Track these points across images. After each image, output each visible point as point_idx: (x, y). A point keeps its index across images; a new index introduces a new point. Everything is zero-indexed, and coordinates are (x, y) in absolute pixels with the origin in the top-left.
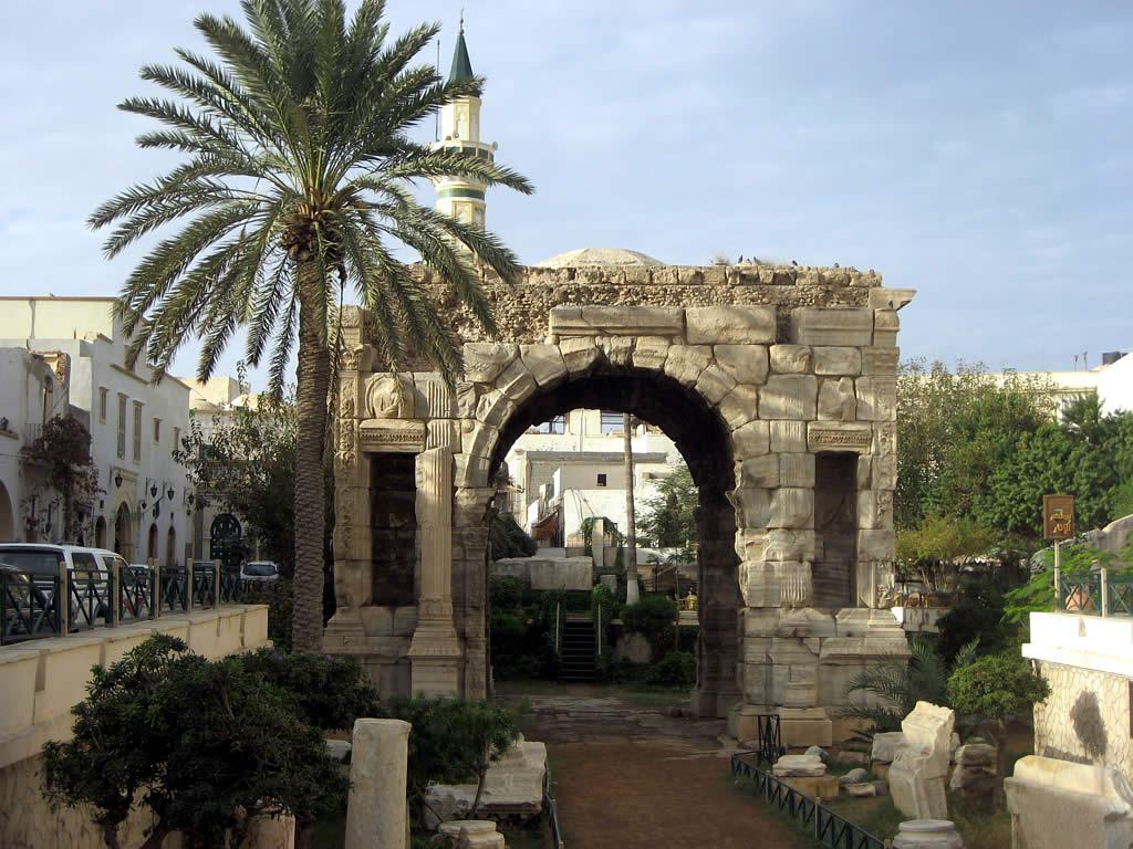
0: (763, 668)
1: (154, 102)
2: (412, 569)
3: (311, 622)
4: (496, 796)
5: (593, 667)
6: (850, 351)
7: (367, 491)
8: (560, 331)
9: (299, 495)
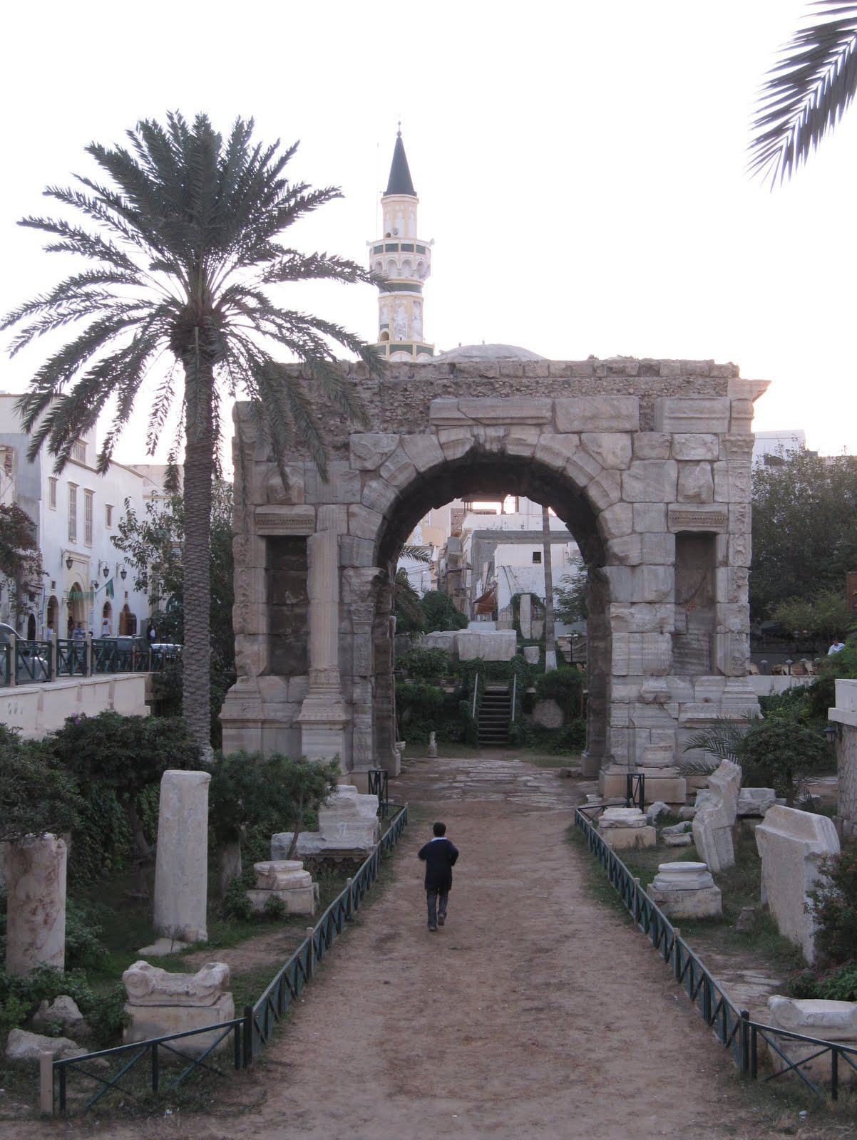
2: (306, 641)
3: (199, 689)
4: (330, 842)
6: (709, 438)
9: (187, 576)
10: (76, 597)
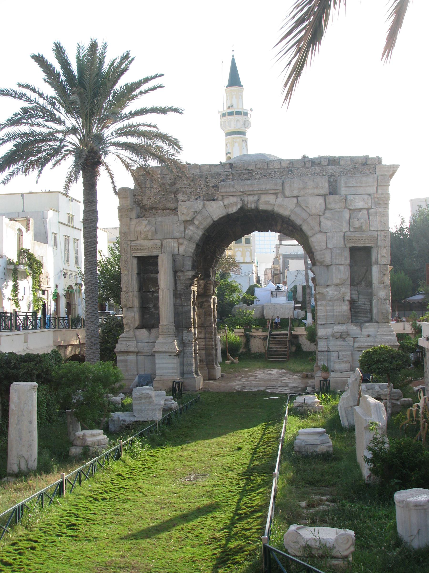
0: (326, 353)
6: (366, 197)
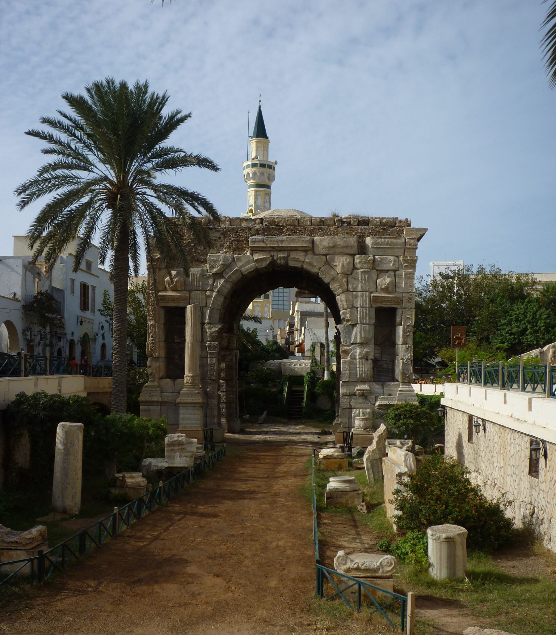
0: (348, 410)
1: (42, 132)
5: (301, 411)
7: (162, 325)
8: (253, 249)
10: (85, 340)
